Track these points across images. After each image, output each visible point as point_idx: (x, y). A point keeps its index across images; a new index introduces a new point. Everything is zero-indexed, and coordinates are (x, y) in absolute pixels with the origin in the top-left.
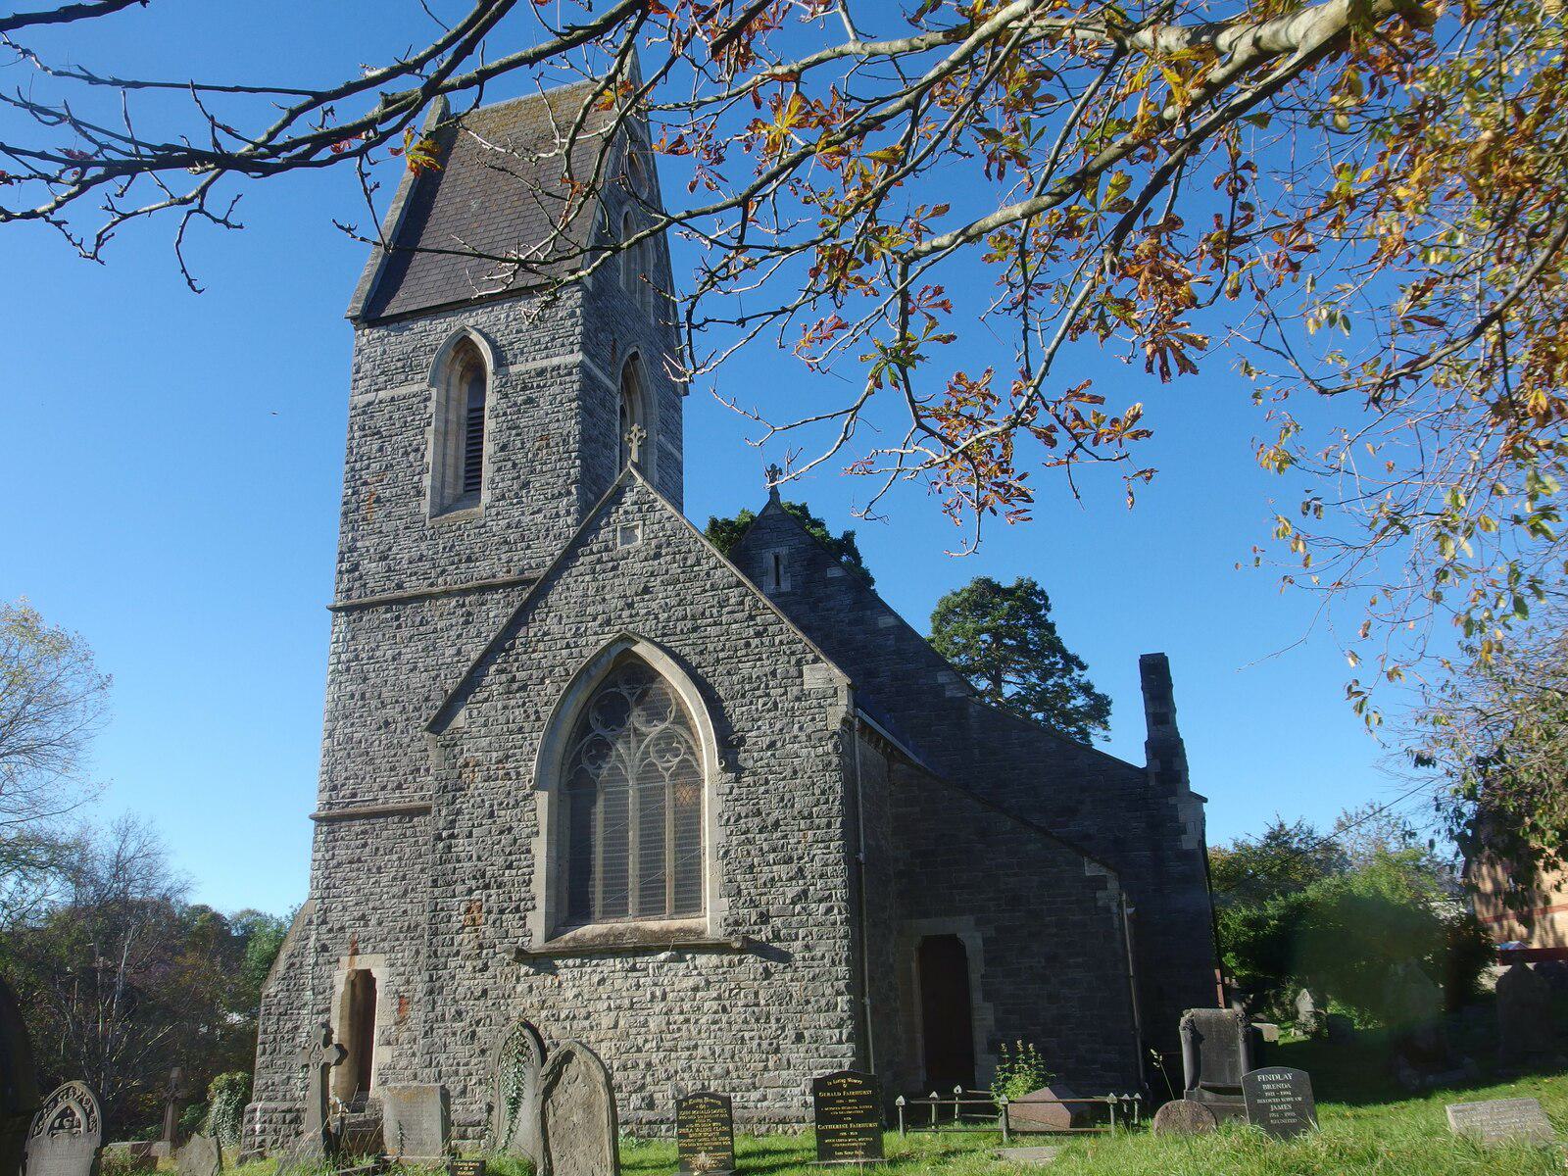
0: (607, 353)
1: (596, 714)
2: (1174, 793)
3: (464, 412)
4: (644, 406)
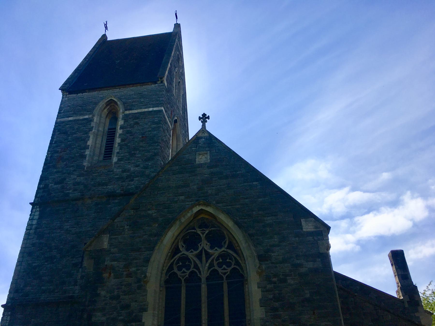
0: (170, 112)
1: (182, 243)
2: (417, 311)
3: (106, 129)
4: (177, 142)
